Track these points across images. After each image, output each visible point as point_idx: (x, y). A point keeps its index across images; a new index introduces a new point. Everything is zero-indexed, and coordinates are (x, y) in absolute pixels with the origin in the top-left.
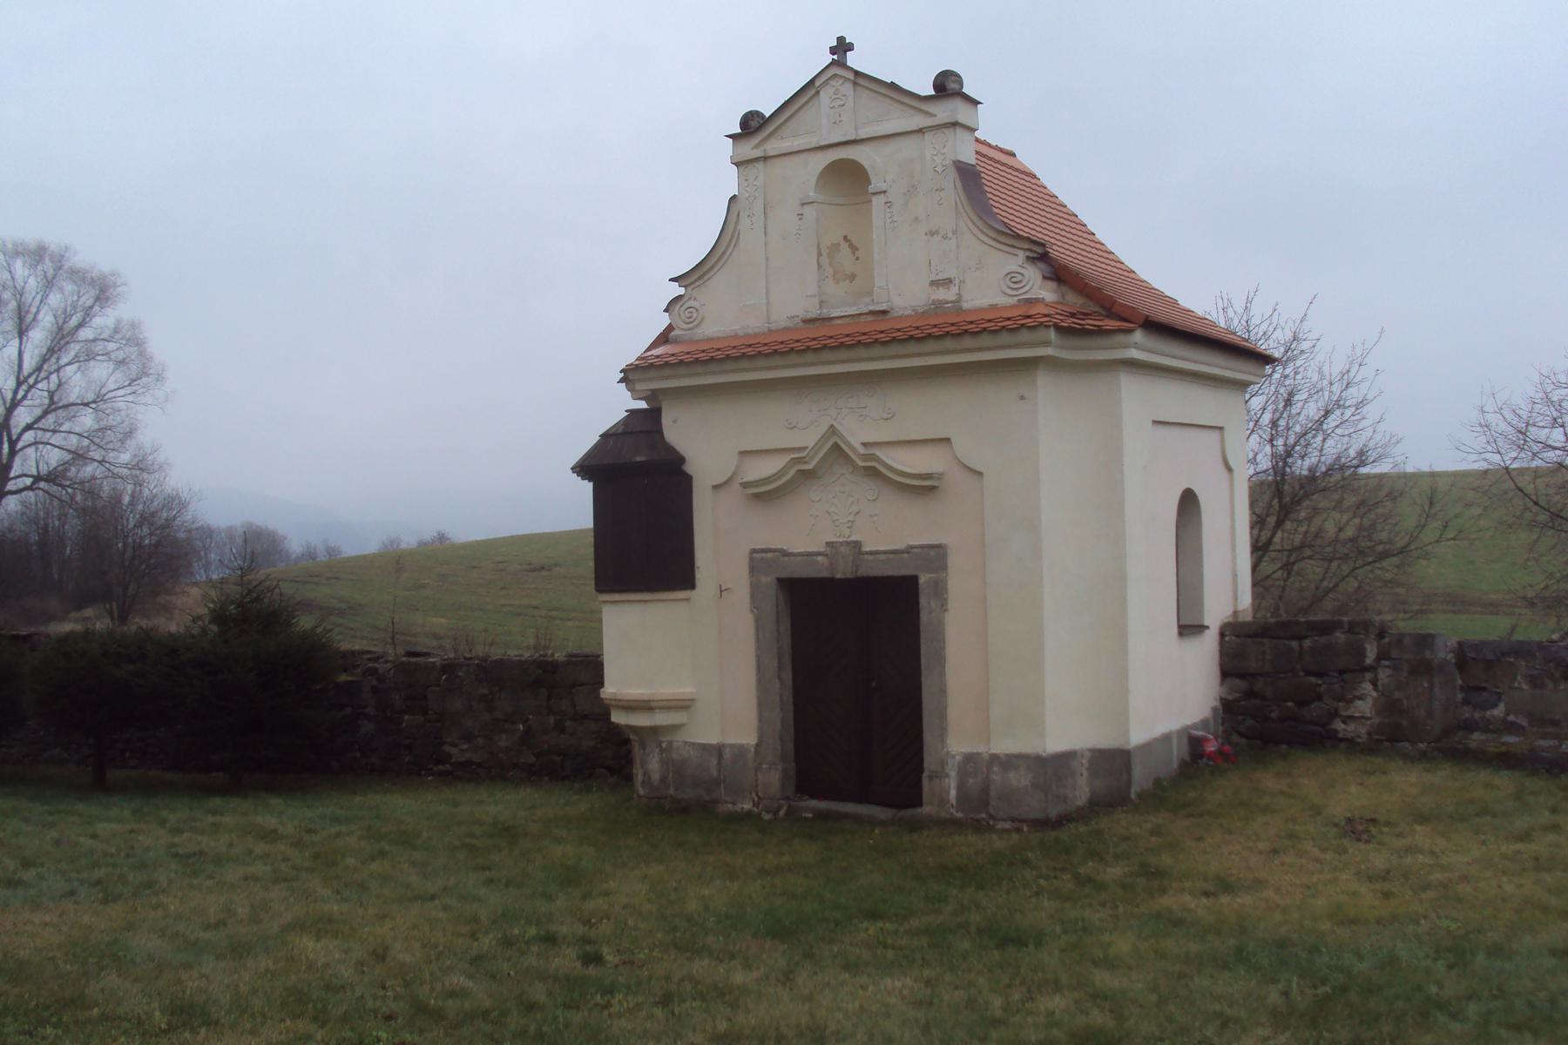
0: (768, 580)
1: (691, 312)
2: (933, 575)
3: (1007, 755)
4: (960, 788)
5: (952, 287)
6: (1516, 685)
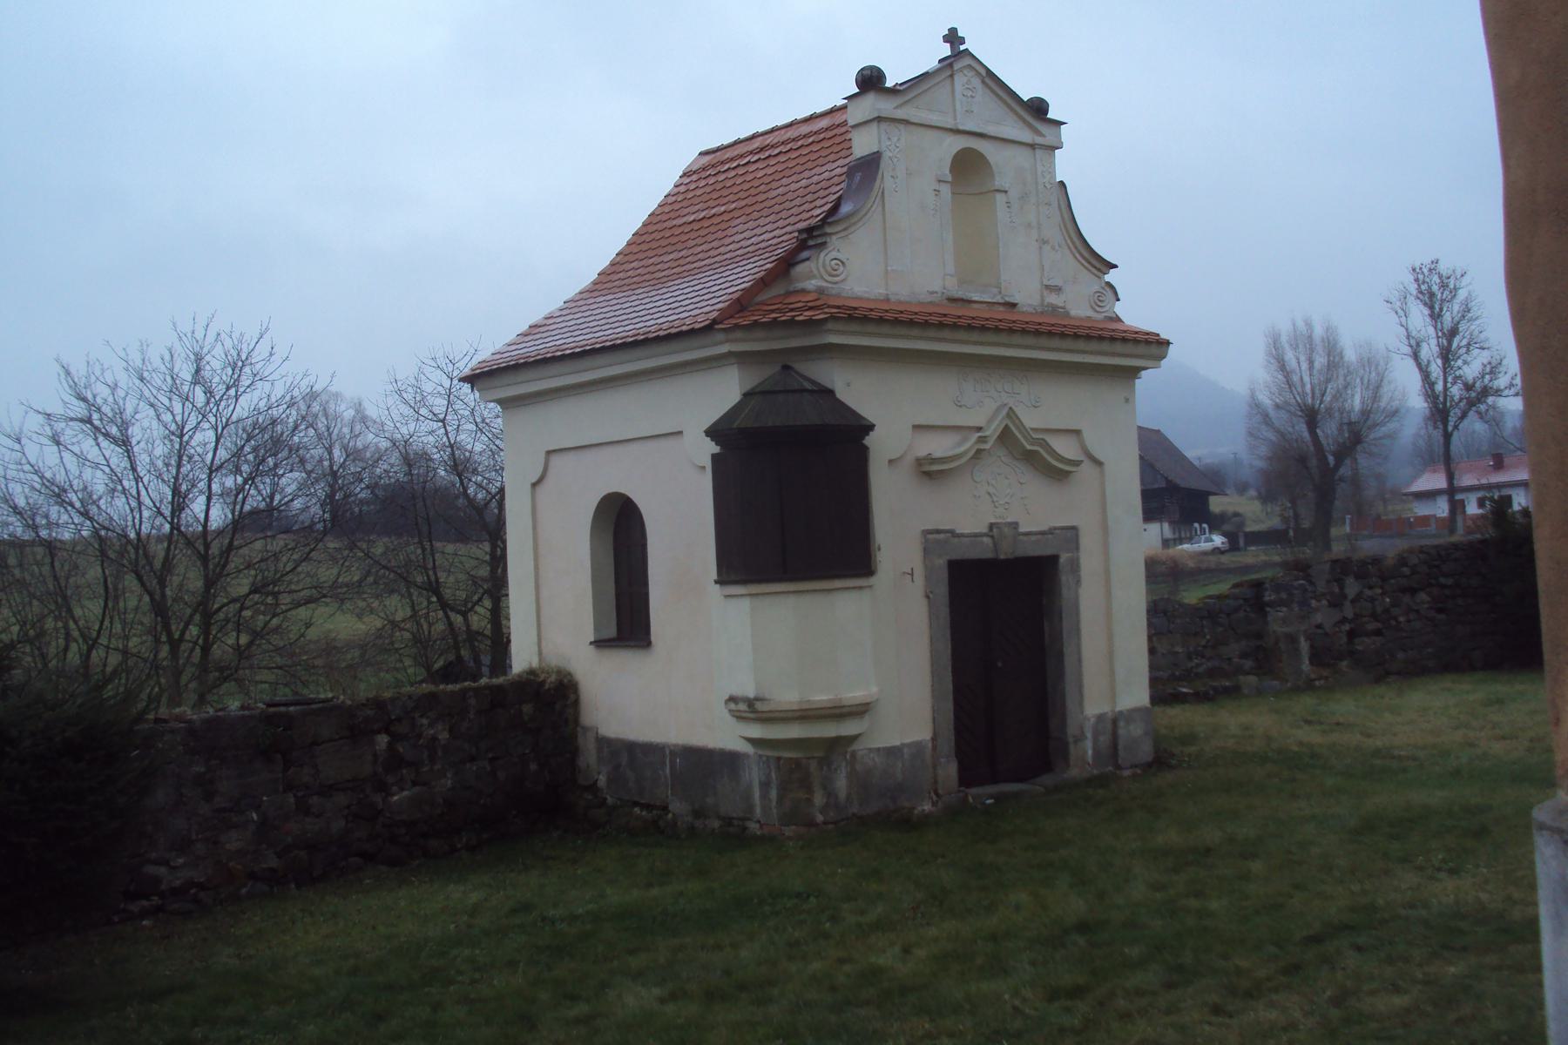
0: (941, 562)
4: (1094, 749)
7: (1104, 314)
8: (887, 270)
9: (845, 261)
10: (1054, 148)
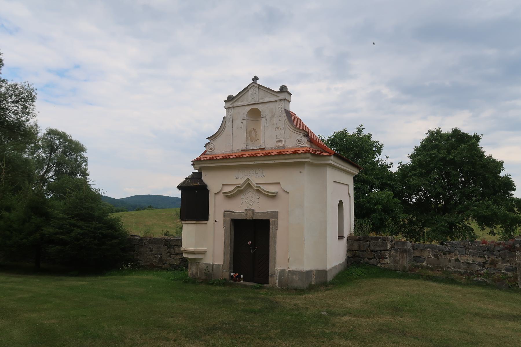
0: (228, 219)
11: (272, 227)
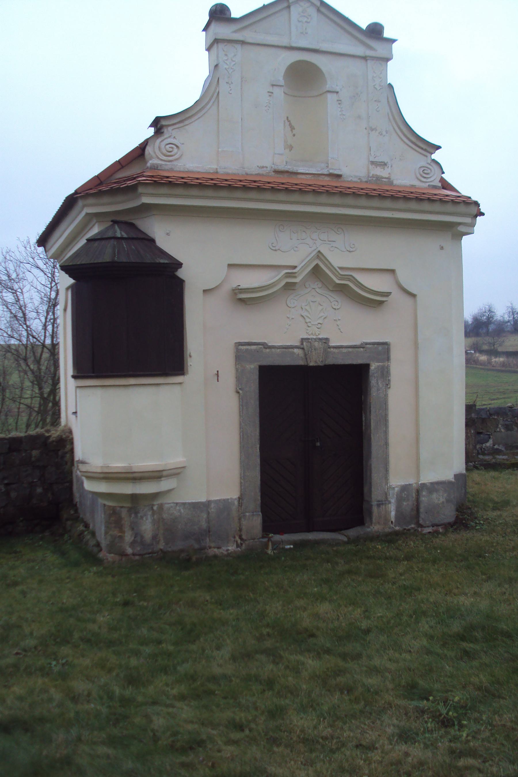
0: (252, 367)
1: (172, 148)
2: (380, 364)
3: (432, 483)
5: (386, 168)
6: (498, 430)
7: (428, 184)
8: (218, 151)
9: (179, 145)
10: (387, 59)
11: (378, 384)
